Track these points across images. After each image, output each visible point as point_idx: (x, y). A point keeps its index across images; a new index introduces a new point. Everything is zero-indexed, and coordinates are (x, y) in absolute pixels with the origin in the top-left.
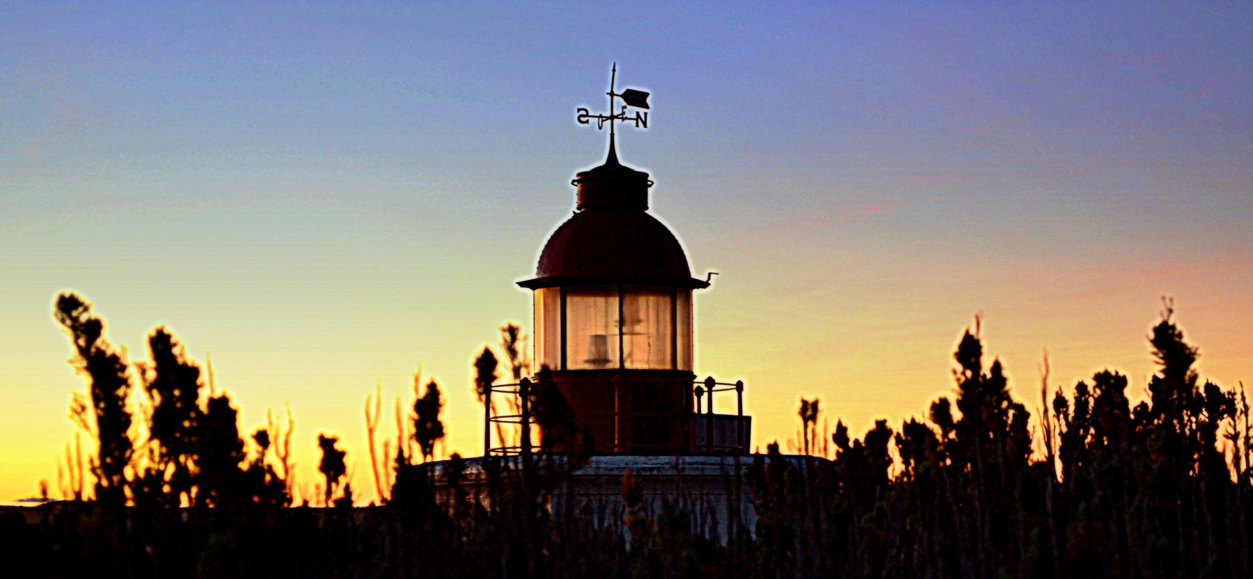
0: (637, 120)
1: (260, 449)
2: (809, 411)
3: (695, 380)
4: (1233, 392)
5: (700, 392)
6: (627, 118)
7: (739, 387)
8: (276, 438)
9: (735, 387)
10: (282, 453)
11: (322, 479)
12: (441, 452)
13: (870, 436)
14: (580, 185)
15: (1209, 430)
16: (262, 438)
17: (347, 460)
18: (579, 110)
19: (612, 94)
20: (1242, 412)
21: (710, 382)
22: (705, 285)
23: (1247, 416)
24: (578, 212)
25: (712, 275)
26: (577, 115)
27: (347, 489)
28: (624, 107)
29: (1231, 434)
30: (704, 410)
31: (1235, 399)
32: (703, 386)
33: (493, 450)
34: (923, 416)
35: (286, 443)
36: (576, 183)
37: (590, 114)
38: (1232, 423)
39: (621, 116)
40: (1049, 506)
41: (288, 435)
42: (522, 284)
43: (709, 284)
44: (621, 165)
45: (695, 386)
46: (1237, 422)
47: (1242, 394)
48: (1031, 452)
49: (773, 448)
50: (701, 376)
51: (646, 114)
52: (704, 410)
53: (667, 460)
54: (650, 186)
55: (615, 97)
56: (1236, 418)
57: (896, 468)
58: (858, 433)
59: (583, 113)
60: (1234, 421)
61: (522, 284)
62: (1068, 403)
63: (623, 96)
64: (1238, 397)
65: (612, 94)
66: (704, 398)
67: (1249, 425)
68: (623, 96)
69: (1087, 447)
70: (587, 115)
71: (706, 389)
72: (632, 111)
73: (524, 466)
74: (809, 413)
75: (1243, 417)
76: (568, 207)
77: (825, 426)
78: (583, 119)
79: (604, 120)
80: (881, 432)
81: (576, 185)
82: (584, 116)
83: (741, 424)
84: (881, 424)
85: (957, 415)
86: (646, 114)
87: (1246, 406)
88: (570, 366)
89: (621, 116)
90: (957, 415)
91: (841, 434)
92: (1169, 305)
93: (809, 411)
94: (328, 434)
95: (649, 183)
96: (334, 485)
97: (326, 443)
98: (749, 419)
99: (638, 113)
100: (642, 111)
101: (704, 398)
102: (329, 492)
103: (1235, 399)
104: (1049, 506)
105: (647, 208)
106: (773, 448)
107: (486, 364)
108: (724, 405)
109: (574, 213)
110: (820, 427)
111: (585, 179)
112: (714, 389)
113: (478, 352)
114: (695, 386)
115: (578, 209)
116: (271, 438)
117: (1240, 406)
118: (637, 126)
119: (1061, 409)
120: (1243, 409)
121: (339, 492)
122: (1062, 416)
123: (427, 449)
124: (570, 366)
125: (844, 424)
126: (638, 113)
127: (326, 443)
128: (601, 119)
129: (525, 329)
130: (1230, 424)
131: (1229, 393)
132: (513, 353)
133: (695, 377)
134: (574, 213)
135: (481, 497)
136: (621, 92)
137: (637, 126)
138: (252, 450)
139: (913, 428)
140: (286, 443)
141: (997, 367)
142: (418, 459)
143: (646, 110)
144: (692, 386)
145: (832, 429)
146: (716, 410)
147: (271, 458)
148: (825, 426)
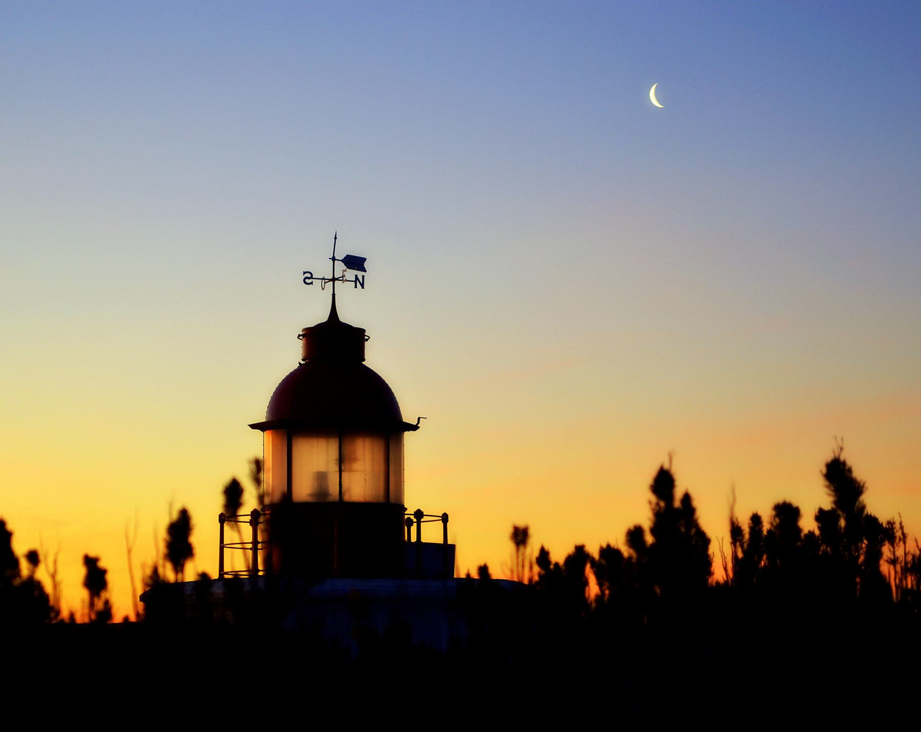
1: (31, 567)
2: (520, 536)
3: (406, 513)
4: (892, 521)
5: (410, 523)
6: (322, 279)
7: (445, 518)
8: (46, 557)
9: (441, 518)
10: (51, 569)
11: (84, 594)
12: (190, 573)
13: (569, 559)
14: (304, 338)
15: (875, 555)
16: (33, 558)
17: (110, 577)
18: (305, 273)
19: (334, 259)
20: (900, 539)
21: (419, 514)
22: (415, 428)
23: (905, 543)
24: (303, 362)
27: (107, 602)
28: (345, 271)
29: (891, 559)
30: (414, 539)
31: (895, 528)
32: (412, 517)
33: (227, 573)
34: (619, 542)
35: (55, 562)
36: (301, 337)
38: (892, 549)
39: (326, 281)
41: (56, 555)
42: (253, 426)
43: (419, 427)
45: (406, 517)
46: (896, 549)
47: (901, 524)
48: (711, 574)
49: (483, 570)
50: (411, 505)
51: (363, 276)
52: (414, 539)
53: (521, 555)
54: (367, 340)
55: (336, 261)
56: (895, 545)
57: (593, 589)
58: (558, 556)
59: (309, 275)
60: (894, 548)
61: (253, 426)
62: (744, 532)
63: (343, 261)
64: (897, 526)
65: (334, 259)
66: (414, 528)
67: (907, 551)
68: (343, 261)
70: (311, 278)
71: (415, 520)
72: (351, 274)
73: (54, 624)
74: (520, 538)
75: (901, 544)
77: (532, 550)
78: (307, 281)
79: (327, 282)
80: (579, 555)
81: (301, 339)
82: (308, 278)
83: (446, 552)
84: (580, 549)
85: (649, 539)
86: (363, 276)
87: (903, 534)
88: (422, 523)
89: (341, 279)
90: (649, 539)
91: (544, 555)
92: (840, 444)
93: (520, 536)
94: (92, 554)
95: (366, 337)
96: (96, 600)
97: (91, 563)
99: (356, 276)
100: (360, 274)
101: (414, 528)
102: (92, 605)
103: (895, 528)
105: (364, 360)
106: (483, 570)
107: (233, 492)
108: (431, 534)
109: (300, 364)
110: (528, 550)
112: (422, 520)
113: (225, 480)
114: (406, 517)
115: (303, 360)
116: (42, 557)
117: (899, 534)
118: (356, 287)
119: (738, 538)
120: (902, 537)
121: (99, 605)
122: (738, 544)
123: (179, 567)
124: (422, 523)
125: (546, 548)
126: (356, 276)
127: (91, 563)
128: (323, 281)
129: (269, 464)
130: (890, 550)
131: (889, 523)
132: (257, 481)
133: (406, 509)
134: (300, 364)
137: (356, 287)
138: (25, 567)
139: (608, 552)
140: (55, 562)
141: (687, 498)
142: (169, 574)
143: (363, 273)
144: (404, 517)
145: (536, 553)
146: (425, 539)
147: (42, 574)
148: (532, 550)
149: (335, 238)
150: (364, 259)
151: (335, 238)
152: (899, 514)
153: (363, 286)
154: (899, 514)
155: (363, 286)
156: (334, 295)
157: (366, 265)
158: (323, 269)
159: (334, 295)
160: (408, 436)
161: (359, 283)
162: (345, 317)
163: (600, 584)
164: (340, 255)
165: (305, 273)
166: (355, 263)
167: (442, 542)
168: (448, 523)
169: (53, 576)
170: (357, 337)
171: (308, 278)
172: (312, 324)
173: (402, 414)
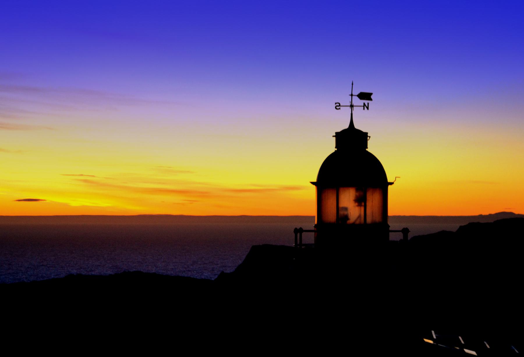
0: (364, 107)
18: (336, 104)
19: (352, 95)
25: (397, 178)
26: (335, 106)
37: (341, 105)
40: (444, 346)
44: (356, 129)
51: (368, 104)
59: (338, 105)
65: (352, 95)
69: (435, 344)
70: (340, 106)
72: (361, 102)
76: (331, 148)
78: (337, 108)
82: (338, 106)
86: (368, 104)
88: (390, 233)
98: (336, 133)
99: (364, 104)
100: (366, 102)
104: (444, 346)
105: (367, 148)
111: (338, 136)
118: (364, 109)
124: (390, 233)
126: (364, 104)
135: (294, 245)
136: (357, 93)
137: (364, 109)
149: (352, 84)
150: (371, 94)
151: (352, 84)
153: (368, 108)
156: (188, 172)
157: (372, 97)
161: (366, 107)
162: (357, 126)
164: (356, 92)
165: (336, 104)
166: (365, 96)
167: (313, 233)
170: (363, 137)
171: (338, 106)
172: (339, 130)
173: (40, 215)
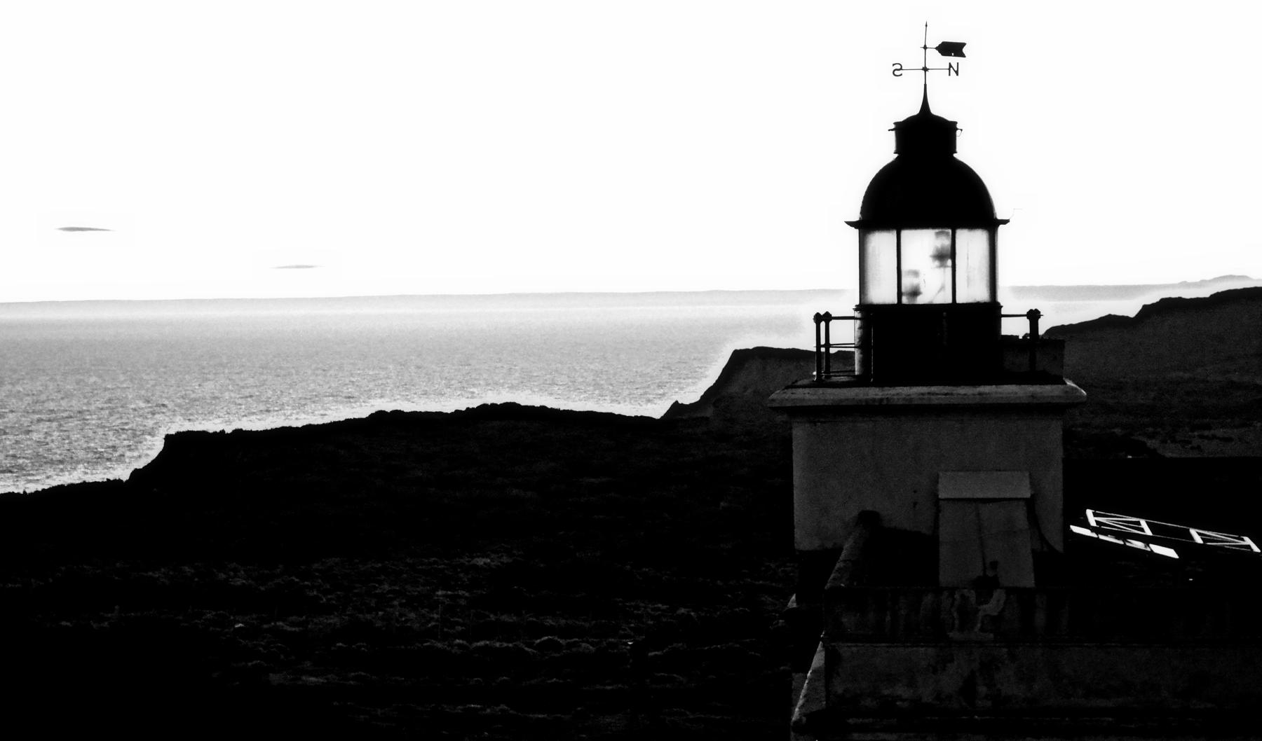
19: (925, 48)
22: (1005, 222)
59: (899, 67)
63: (937, 48)
67: (949, 262)
68: (937, 48)
70: (901, 69)
78: (896, 73)
124: (1003, 319)
149: (926, 26)
151: (926, 26)
152: (949, 75)
153: (957, 73)
154: (949, 75)
155: (957, 73)
156: (925, 85)
157: (965, 50)
158: (914, 59)
159: (925, 85)
160: (1001, 227)
162: (936, 110)
163: (1070, 386)
165: (894, 65)
166: (951, 49)
168: (1040, 320)
169: (163, 413)
